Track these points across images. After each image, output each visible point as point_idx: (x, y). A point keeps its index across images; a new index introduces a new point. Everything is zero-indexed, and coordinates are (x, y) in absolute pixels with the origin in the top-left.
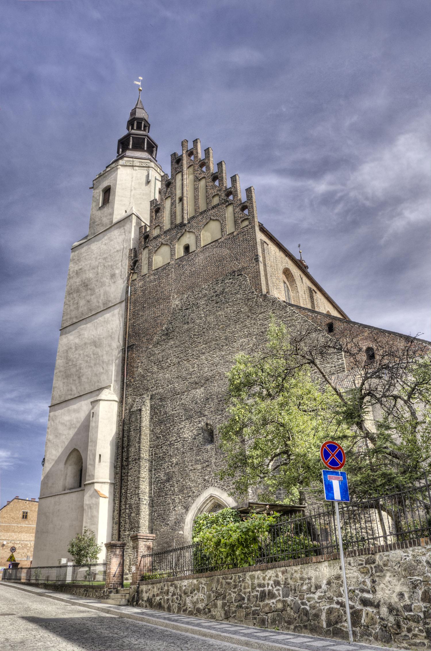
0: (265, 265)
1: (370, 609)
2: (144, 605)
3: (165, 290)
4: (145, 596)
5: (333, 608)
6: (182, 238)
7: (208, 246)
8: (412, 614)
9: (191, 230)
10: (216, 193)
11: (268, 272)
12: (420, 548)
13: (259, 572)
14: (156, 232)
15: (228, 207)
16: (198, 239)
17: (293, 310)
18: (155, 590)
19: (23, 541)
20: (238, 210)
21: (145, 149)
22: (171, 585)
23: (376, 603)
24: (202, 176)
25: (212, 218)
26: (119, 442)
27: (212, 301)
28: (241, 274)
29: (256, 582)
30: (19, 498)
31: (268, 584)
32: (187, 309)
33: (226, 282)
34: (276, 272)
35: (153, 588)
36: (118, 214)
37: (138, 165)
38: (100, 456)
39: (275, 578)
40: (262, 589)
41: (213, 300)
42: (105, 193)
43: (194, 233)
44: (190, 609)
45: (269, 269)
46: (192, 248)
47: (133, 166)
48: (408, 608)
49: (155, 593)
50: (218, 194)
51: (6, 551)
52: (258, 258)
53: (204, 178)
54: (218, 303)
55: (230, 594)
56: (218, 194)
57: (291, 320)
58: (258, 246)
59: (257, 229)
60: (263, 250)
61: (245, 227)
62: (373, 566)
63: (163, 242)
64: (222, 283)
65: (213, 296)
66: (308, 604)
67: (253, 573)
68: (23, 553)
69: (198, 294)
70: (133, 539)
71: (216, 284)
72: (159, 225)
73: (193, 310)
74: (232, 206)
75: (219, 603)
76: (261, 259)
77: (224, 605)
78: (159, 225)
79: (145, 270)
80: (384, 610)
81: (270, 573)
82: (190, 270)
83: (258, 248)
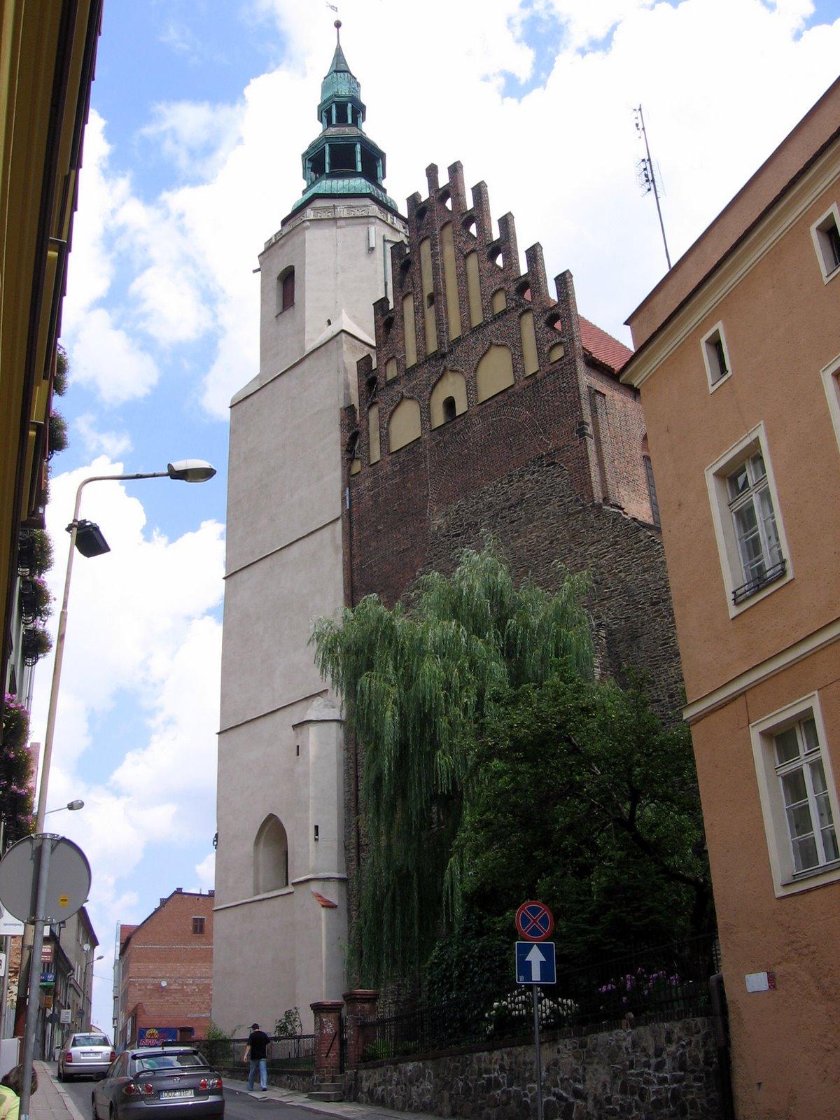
0: (598, 442)
1: (579, 1102)
2: (364, 1099)
3: (416, 495)
4: (365, 1085)
5: (550, 1100)
6: (439, 385)
7: (490, 402)
8: (611, 1107)
9: (455, 368)
10: (498, 287)
11: (605, 456)
12: (622, 1031)
13: (486, 1053)
14: (392, 371)
15: (524, 317)
16: (472, 388)
17: (651, 536)
18: (377, 1076)
19: (200, 978)
20: (542, 323)
21: (359, 169)
22: (395, 1070)
23: (584, 1095)
24: (471, 247)
25: (494, 341)
26: (349, 799)
27: (501, 518)
28: (553, 463)
29: (483, 1066)
30: (183, 891)
31: (494, 1069)
32: (458, 535)
33: (526, 479)
34: (627, 447)
35: (375, 1074)
36: (315, 335)
37: (345, 215)
38: (317, 827)
39: (501, 1062)
40: (488, 1076)
41: (505, 517)
42: (284, 284)
43: (462, 373)
44: (416, 1104)
45: (607, 448)
46: (461, 408)
47: (335, 219)
48: (608, 1100)
49: (377, 1082)
50: (501, 289)
51: (167, 1001)
52: (583, 429)
53: (473, 251)
54: (513, 522)
55: (457, 1083)
56: (501, 289)
57: (647, 557)
58: (582, 402)
59: (581, 365)
60: (594, 411)
61: (556, 361)
62: (585, 1050)
63: (405, 394)
64: (519, 481)
65: (503, 509)
66: (530, 1095)
67: (481, 1054)
68: (203, 1003)
69: (477, 503)
70: (347, 998)
71: (509, 482)
72: (394, 357)
73: (470, 537)
74: (531, 315)
75: (446, 1094)
76: (590, 430)
77: (451, 1096)
78: (394, 357)
79: (376, 455)
80: (590, 1103)
81: (496, 1054)
82: (459, 453)
83: (584, 406)
